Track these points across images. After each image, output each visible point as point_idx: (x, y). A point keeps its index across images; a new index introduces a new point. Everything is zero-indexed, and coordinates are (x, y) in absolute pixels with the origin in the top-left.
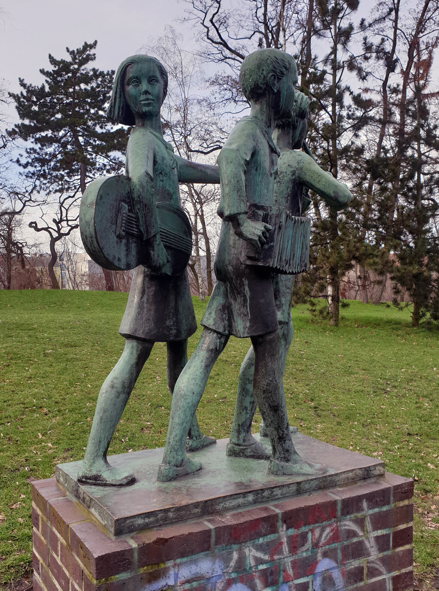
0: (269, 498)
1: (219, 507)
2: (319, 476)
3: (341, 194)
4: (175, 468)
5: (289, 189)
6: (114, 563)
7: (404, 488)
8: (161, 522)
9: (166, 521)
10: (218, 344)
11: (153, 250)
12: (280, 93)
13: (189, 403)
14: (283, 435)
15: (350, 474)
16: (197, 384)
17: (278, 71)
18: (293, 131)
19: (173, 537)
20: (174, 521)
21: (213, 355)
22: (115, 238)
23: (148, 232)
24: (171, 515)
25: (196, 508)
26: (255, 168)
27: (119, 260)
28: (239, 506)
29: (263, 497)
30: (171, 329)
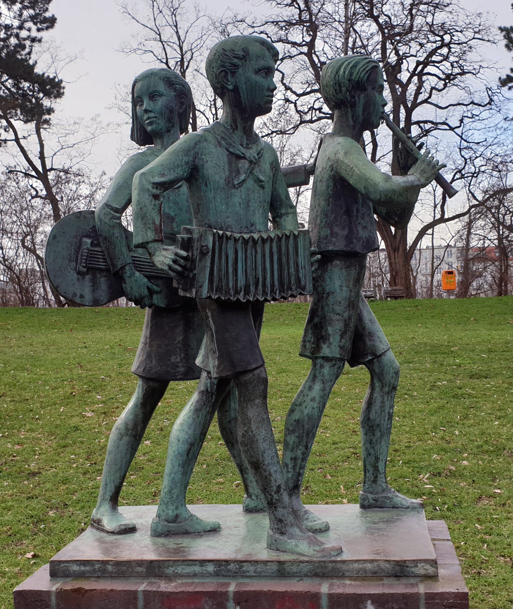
0: (237, 573)
1: (170, 571)
2: (314, 560)
3: (372, 189)
4: (166, 523)
5: (330, 189)
6: (32, 601)
7: (448, 599)
8: (99, 574)
9: (104, 573)
10: (209, 385)
11: (125, 283)
12: (238, 89)
13: (174, 452)
14: (271, 499)
15: (369, 566)
16: (183, 430)
17: (227, 64)
18: (351, 109)
19: (94, 590)
20: (113, 575)
21: (204, 397)
22: (75, 275)
23: (113, 265)
24: (110, 568)
25: (140, 566)
26: (204, 183)
27: (82, 296)
28: (195, 575)
29: (229, 571)
30: (178, 366)
